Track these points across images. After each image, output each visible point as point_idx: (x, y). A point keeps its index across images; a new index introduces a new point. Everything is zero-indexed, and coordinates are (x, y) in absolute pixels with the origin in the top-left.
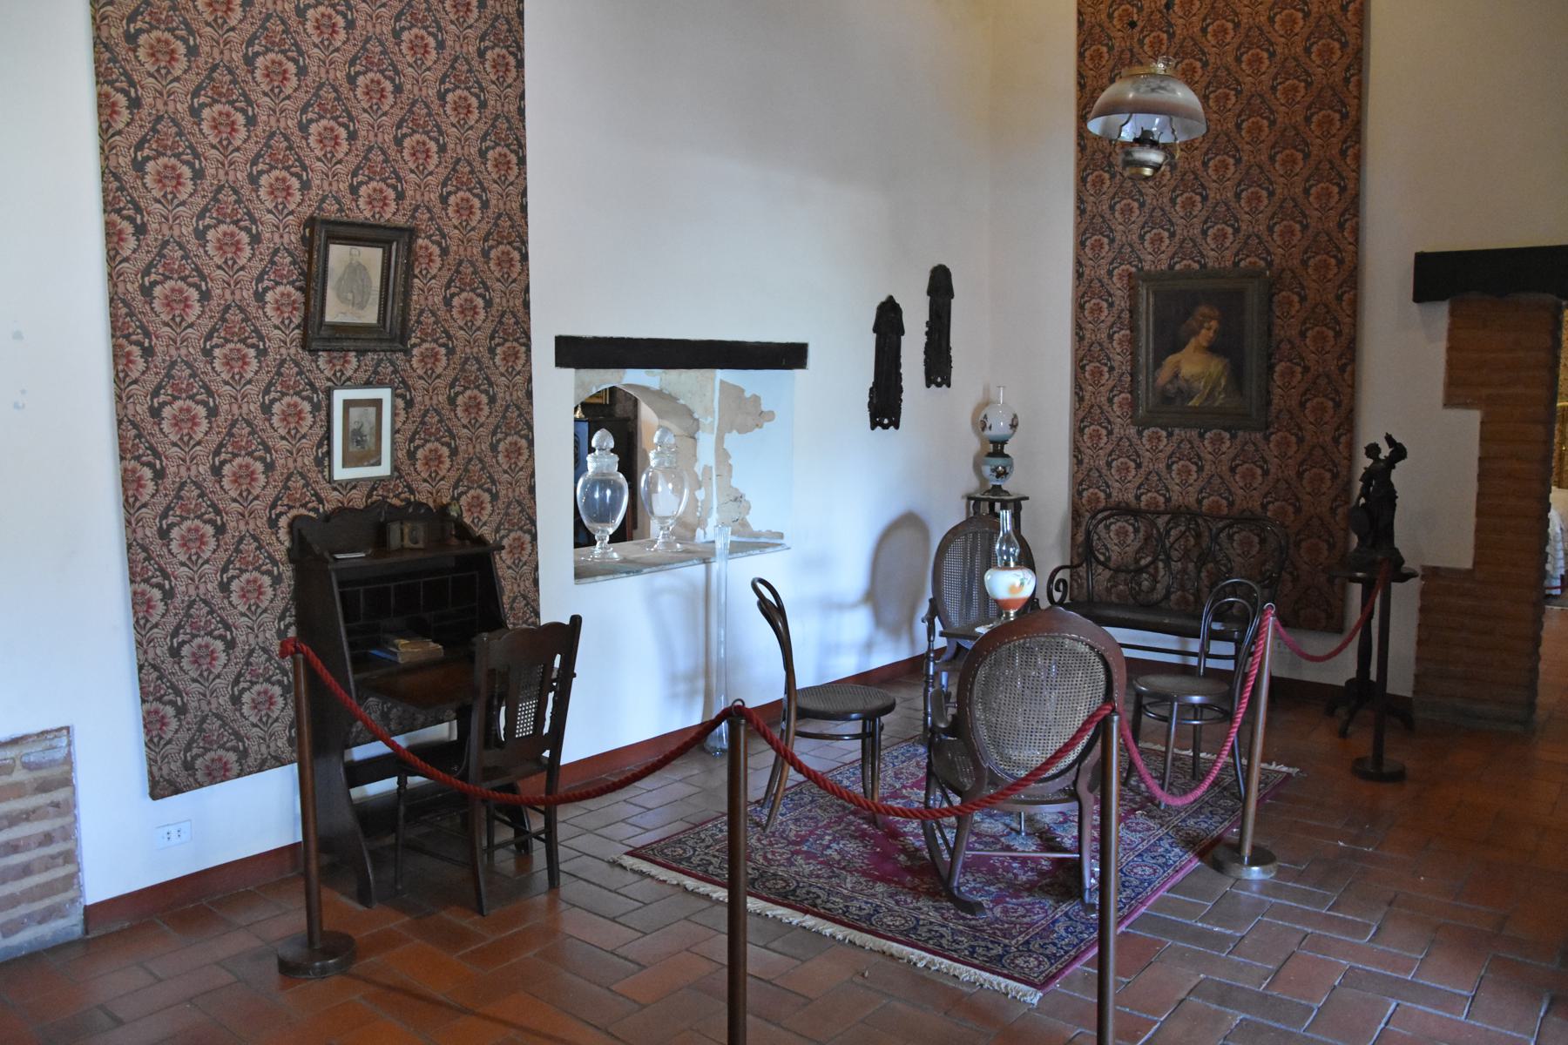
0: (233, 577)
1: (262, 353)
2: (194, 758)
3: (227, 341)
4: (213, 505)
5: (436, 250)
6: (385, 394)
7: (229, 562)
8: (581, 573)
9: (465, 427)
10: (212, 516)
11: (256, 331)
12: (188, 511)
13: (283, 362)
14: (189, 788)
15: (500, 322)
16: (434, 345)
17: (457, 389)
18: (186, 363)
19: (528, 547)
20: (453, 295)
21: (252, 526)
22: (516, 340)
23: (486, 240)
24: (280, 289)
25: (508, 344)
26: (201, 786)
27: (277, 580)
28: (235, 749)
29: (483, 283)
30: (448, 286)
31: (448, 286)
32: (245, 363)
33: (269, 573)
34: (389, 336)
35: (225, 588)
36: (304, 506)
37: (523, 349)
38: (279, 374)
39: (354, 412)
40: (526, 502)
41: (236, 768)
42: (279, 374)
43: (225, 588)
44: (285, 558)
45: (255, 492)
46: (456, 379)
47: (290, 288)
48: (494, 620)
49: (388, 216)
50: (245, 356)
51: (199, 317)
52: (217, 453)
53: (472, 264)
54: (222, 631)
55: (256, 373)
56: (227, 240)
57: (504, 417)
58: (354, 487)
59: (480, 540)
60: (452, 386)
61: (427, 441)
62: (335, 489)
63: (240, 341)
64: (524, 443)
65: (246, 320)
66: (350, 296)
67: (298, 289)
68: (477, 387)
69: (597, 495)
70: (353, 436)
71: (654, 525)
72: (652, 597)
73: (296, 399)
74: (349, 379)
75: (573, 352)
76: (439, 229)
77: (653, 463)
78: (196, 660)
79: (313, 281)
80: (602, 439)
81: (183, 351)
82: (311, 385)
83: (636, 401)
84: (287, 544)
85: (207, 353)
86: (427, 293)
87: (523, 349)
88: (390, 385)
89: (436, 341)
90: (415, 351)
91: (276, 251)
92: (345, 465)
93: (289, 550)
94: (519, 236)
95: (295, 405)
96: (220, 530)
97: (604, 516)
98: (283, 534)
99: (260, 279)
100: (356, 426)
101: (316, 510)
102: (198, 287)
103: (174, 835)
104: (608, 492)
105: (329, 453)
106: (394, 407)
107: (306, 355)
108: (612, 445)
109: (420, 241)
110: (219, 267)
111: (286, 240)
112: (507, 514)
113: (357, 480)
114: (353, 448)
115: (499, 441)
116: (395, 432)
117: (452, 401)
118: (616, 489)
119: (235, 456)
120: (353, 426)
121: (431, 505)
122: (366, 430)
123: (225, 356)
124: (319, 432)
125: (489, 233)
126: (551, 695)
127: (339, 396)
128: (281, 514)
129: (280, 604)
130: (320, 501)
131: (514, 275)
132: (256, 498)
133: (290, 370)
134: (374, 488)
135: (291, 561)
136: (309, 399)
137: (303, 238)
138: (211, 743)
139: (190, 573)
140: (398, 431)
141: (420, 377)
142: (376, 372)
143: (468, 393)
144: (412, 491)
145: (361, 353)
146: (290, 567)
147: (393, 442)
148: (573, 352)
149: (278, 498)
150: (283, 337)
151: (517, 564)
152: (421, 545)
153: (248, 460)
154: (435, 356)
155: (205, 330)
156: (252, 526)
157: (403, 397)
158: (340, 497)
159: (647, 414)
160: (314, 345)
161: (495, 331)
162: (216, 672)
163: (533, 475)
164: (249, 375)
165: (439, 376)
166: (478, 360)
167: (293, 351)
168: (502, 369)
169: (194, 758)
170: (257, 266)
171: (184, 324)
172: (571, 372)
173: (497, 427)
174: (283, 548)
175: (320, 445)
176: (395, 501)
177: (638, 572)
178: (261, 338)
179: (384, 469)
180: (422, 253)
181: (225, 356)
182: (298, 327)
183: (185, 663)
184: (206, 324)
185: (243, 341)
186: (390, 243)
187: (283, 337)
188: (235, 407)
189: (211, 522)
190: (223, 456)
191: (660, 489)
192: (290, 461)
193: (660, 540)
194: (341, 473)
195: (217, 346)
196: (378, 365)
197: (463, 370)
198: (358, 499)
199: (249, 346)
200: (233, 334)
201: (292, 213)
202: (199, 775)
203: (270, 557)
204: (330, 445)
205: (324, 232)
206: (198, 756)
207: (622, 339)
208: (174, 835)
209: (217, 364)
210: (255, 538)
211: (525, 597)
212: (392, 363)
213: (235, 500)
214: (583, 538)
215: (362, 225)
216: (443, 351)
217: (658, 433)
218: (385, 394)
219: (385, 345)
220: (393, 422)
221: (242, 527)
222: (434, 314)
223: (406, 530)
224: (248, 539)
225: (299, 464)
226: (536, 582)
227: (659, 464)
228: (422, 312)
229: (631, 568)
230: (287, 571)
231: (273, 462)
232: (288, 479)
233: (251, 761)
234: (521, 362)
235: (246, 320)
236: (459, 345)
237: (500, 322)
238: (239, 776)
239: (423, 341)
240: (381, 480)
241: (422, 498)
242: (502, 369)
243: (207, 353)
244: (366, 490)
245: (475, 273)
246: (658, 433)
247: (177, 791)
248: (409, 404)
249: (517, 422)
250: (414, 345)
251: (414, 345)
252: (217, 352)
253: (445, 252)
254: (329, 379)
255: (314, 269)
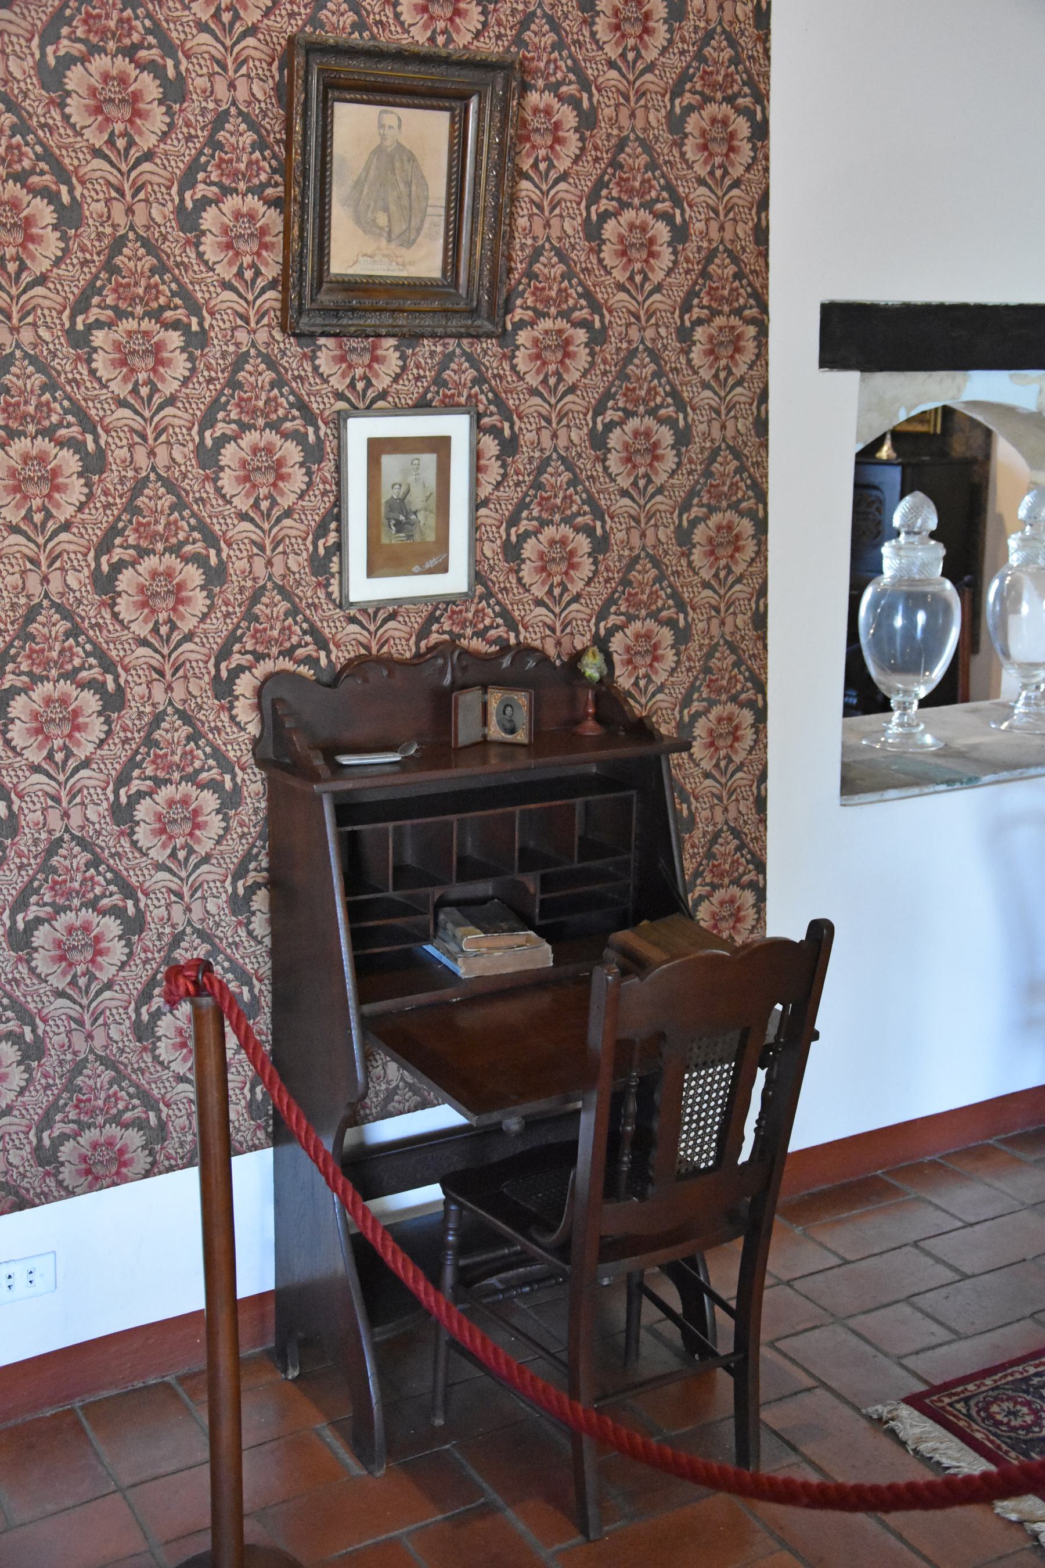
0: (140, 795)
1: (197, 342)
2: (59, 1141)
3: (121, 314)
4: (99, 653)
5: (568, 117)
6: (456, 427)
7: (132, 764)
8: (858, 780)
9: (624, 493)
10: (95, 673)
11: (183, 293)
12: (46, 664)
13: (242, 359)
14: (47, 1198)
15: (704, 274)
16: (561, 324)
17: (610, 415)
18: (33, 360)
19: (748, 735)
20: (604, 217)
21: (178, 694)
22: (738, 312)
23: (677, 92)
24: (231, 203)
25: (719, 321)
26: (71, 1193)
27: (231, 800)
28: (140, 1124)
29: (669, 188)
30: (594, 197)
31: (594, 197)
32: (160, 362)
33: (215, 786)
34: (461, 307)
35: (122, 814)
36: (288, 653)
37: (752, 331)
38: (233, 384)
39: (390, 463)
40: (748, 646)
41: (142, 1160)
42: (233, 384)
43: (122, 814)
44: (248, 758)
45: (186, 625)
46: (607, 395)
47: (253, 202)
48: (660, 897)
49: (463, 39)
50: (159, 347)
51: (57, 262)
52: (104, 546)
53: (647, 147)
54: (116, 899)
55: (185, 382)
56: (113, 90)
57: (708, 474)
58: (392, 616)
59: (642, 730)
60: (599, 409)
61: (544, 523)
62: (352, 620)
63: (149, 314)
64: (746, 526)
65: (160, 269)
66: (382, 219)
67: (271, 203)
68: (652, 412)
69: (899, 622)
70: (391, 516)
71: (1010, 680)
72: (998, 830)
73: (270, 436)
74: (383, 395)
75: (858, 336)
76: (576, 69)
77: (1014, 559)
78: (63, 956)
79: (304, 184)
80: (915, 511)
81: (27, 336)
82: (303, 407)
83: (988, 434)
84: (254, 729)
85: (79, 340)
86: (549, 212)
87: (752, 331)
88: (470, 407)
89: (564, 315)
90: (523, 337)
91: (221, 119)
92: (372, 571)
93: (256, 742)
94: (750, 82)
95: (269, 450)
96: (113, 702)
97: (913, 658)
98: (245, 711)
99: (188, 181)
100: (395, 493)
101: (311, 661)
102: (52, 197)
103: (20, 1279)
104: (921, 617)
105: (339, 548)
106: (477, 455)
107: (293, 347)
108: (933, 524)
109: (533, 98)
110: (97, 153)
111: (242, 93)
112: (707, 670)
113: (399, 602)
114: (390, 538)
115: (694, 523)
116: (477, 504)
117: (598, 441)
118: (937, 607)
119: (143, 553)
120: (387, 493)
121: (551, 650)
122: (417, 500)
123: (118, 346)
124: (318, 504)
125: (684, 77)
126: (761, 1075)
127: (360, 431)
128: (240, 669)
129: (235, 848)
130: (322, 643)
131: (737, 171)
132: (189, 637)
133: (257, 377)
134: (432, 619)
135: (261, 763)
136: (299, 438)
137: (277, 88)
138: (92, 1112)
139: (51, 787)
140: (485, 503)
141: (533, 392)
142: (439, 382)
143: (633, 423)
144: (512, 625)
145: (409, 338)
146: (260, 774)
147: (475, 526)
148: (858, 336)
149: (233, 638)
150: (240, 306)
151: (725, 768)
152: (521, 736)
153: (170, 560)
154: (565, 346)
155: (72, 292)
156: (178, 694)
157: (495, 431)
158: (363, 636)
159: (1007, 456)
160: (305, 324)
161: (692, 294)
162: (104, 977)
163: (762, 592)
164: (169, 387)
165: (572, 389)
166: (655, 356)
167: (262, 336)
168: (706, 374)
169: (59, 1141)
170: (180, 153)
171: (26, 278)
172: (853, 377)
173: (692, 493)
174: (243, 736)
175: (322, 531)
176: (477, 645)
177: (971, 782)
178: (194, 309)
179: (455, 580)
180: (536, 123)
181: (118, 346)
182: (272, 285)
183: (40, 961)
184: (74, 277)
185: (155, 315)
186: (465, 98)
187: (240, 306)
188: (141, 453)
189: (96, 686)
190: (117, 554)
191: (1025, 608)
192: (259, 563)
193: (1020, 709)
194: (364, 588)
195: (98, 324)
196: (444, 366)
197: (623, 376)
198: (400, 641)
199: (167, 326)
200: (133, 300)
201: (252, 31)
202: (67, 1174)
203: (217, 754)
204: (341, 530)
205: (330, 71)
206: (64, 1137)
207: (964, 307)
208: (20, 1279)
209: (100, 362)
210: (186, 718)
211: (736, 833)
212: (474, 362)
213: (144, 643)
214: (864, 696)
215: (402, 56)
216: (581, 335)
217: (1028, 499)
218: (456, 427)
219: (455, 324)
220: (475, 483)
221: (159, 693)
222: (563, 257)
223: (494, 706)
224: (171, 720)
225: (278, 569)
226: (761, 804)
227: (1027, 561)
228: (537, 253)
229: (957, 769)
230: (254, 784)
231: (222, 566)
232: (255, 599)
233: (172, 1146)
234: (748, 356)
235: (160, 269)
236: (617, 324)
237: (704, 274)
238: (147, 1174)
239: (540, 315)
240: (448, 601)
241: (532, 638)
242: (706, 374)
243: (79, 340)
244: (417, 622)
245: (652, 166)
246: (1028, 499)
247: (22, 1204)
248: (509, 447)
249: (737, 485)
250: (521, 325)
251: (521, 325)
252: (99, 337)
253: (588, 120)
254: (339, 396)
255: (296, 157)
